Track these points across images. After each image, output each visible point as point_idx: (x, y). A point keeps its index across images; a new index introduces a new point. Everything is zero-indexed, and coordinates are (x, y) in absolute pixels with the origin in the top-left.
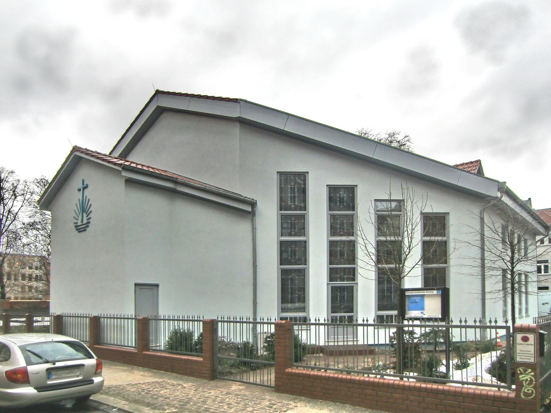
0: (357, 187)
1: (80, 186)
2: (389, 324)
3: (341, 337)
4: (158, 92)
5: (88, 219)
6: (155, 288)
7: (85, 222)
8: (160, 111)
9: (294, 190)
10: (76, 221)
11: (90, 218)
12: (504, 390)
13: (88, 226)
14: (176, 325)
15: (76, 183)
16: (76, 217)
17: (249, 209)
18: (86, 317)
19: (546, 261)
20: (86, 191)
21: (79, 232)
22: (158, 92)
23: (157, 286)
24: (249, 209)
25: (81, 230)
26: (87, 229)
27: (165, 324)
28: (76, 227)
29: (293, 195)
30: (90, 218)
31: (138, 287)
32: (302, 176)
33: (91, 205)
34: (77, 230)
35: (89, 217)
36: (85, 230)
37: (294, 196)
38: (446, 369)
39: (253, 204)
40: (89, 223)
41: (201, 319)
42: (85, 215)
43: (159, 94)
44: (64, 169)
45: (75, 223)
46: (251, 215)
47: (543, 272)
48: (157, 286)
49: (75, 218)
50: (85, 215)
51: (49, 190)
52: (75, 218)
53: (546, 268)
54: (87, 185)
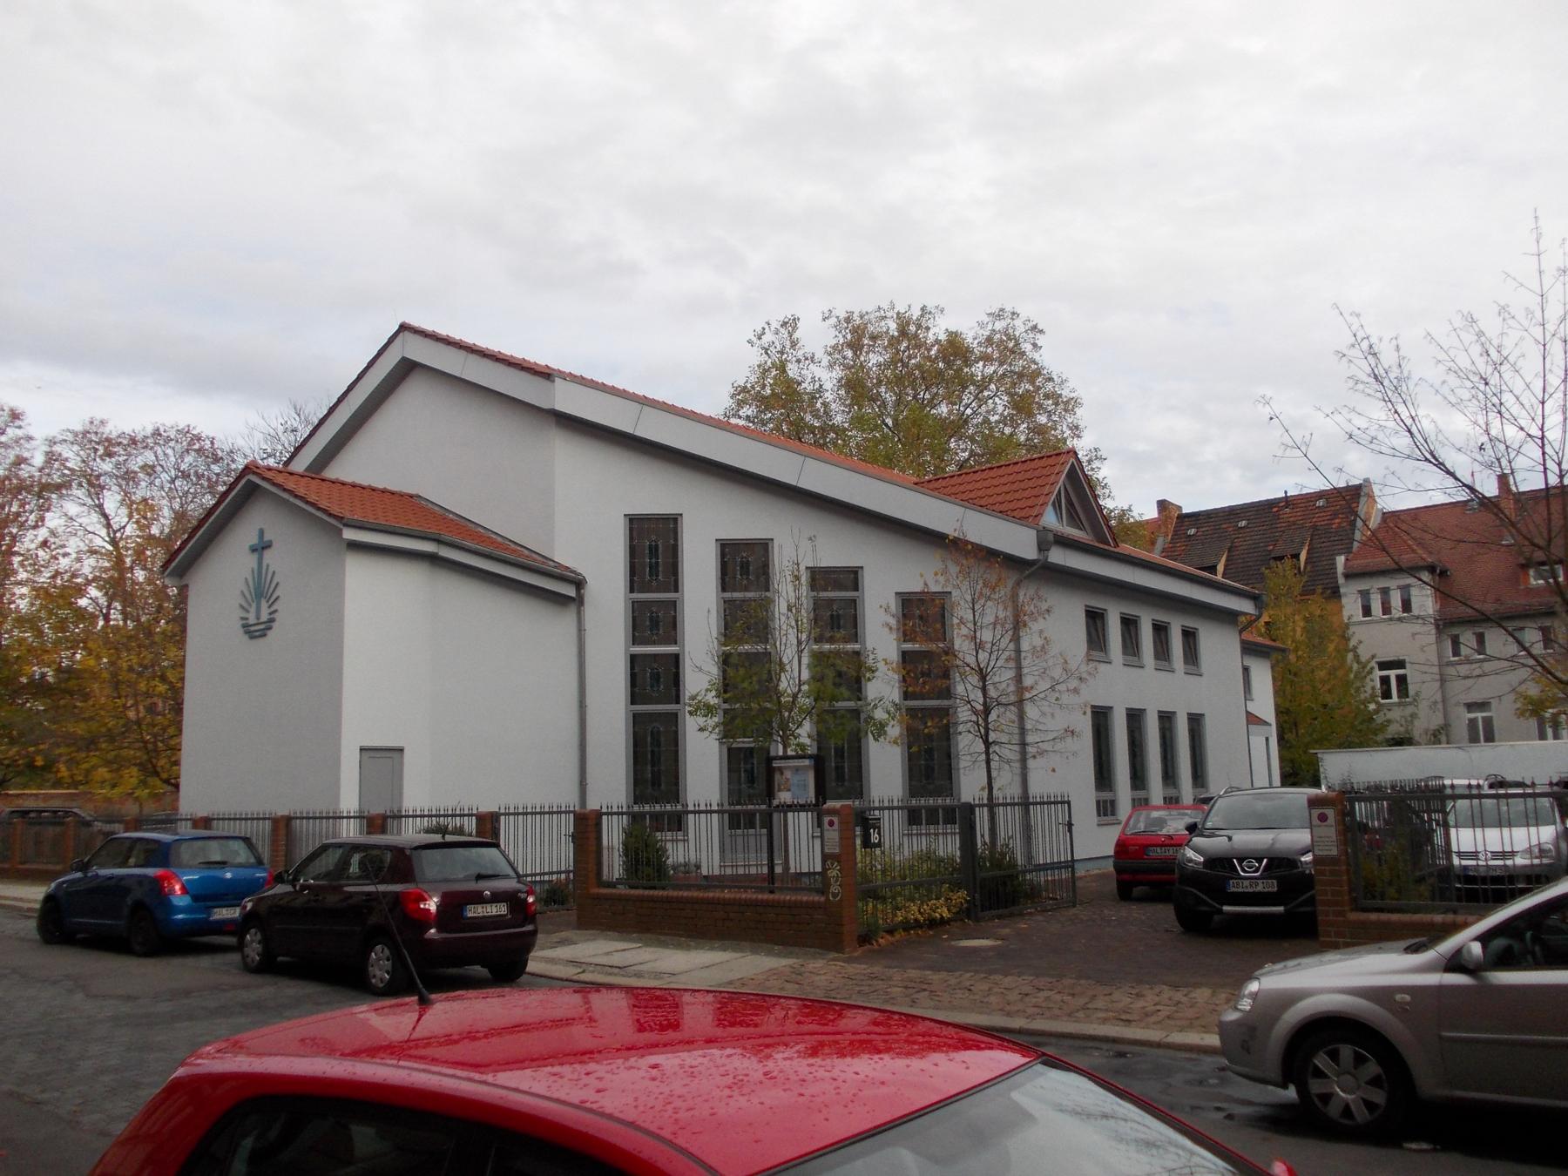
0: (402, 757)
1: (254, 540)
2: (1327, 868)
3: (753, 855)
4: (404, 328)
5: (270, 614)
6: (396, 755)
7: (264, 617)
8: (408, 368)
9: (657, 550)
10: (244, 615)
11: (276, 611)
12: (1236, 1009)
13: (270, 628)
14: (418, 823)
15: (243, 534)
16: (245, 605)
17: (570, 591)
18: (264, 819)
19: (1400, 664)
20: (268, 555)
21: (252, 638)
22: (404, 328)
23: (401, 750)
24: (570, 591)
25: (257, 634)
26: (269, 632)
27: (821, 1152)
28: (244, 626)
29: (654, 560)
30: (276, 611)
31: (364, 753)
32: (672, 522)
33: (277, 584)
34: (246, 633)
35: (272, 609)
36: (265, 635)
37: (657, 563)
38: (401, 794)
39: (579, 583)
40: (272, 620)
41: (475, 812)
42: (264, 605)
43: (406, 333)
44: (222, 507)
45: (242, 618)
46: (573, 608)
47: (1395, 698)
48: (401, 750)
49: (241, 606)
50: (264, 605)
51: (190, 545)
52: (241, 606)
53: (1402, 680)
54: (271, 541)
